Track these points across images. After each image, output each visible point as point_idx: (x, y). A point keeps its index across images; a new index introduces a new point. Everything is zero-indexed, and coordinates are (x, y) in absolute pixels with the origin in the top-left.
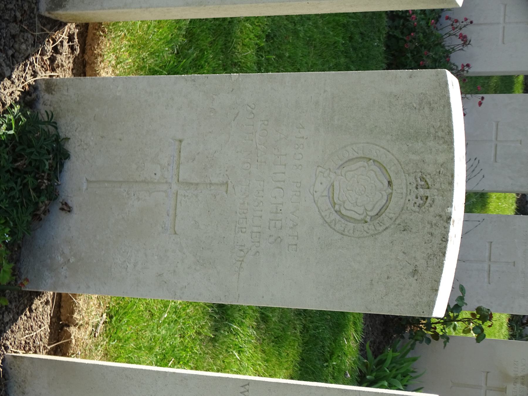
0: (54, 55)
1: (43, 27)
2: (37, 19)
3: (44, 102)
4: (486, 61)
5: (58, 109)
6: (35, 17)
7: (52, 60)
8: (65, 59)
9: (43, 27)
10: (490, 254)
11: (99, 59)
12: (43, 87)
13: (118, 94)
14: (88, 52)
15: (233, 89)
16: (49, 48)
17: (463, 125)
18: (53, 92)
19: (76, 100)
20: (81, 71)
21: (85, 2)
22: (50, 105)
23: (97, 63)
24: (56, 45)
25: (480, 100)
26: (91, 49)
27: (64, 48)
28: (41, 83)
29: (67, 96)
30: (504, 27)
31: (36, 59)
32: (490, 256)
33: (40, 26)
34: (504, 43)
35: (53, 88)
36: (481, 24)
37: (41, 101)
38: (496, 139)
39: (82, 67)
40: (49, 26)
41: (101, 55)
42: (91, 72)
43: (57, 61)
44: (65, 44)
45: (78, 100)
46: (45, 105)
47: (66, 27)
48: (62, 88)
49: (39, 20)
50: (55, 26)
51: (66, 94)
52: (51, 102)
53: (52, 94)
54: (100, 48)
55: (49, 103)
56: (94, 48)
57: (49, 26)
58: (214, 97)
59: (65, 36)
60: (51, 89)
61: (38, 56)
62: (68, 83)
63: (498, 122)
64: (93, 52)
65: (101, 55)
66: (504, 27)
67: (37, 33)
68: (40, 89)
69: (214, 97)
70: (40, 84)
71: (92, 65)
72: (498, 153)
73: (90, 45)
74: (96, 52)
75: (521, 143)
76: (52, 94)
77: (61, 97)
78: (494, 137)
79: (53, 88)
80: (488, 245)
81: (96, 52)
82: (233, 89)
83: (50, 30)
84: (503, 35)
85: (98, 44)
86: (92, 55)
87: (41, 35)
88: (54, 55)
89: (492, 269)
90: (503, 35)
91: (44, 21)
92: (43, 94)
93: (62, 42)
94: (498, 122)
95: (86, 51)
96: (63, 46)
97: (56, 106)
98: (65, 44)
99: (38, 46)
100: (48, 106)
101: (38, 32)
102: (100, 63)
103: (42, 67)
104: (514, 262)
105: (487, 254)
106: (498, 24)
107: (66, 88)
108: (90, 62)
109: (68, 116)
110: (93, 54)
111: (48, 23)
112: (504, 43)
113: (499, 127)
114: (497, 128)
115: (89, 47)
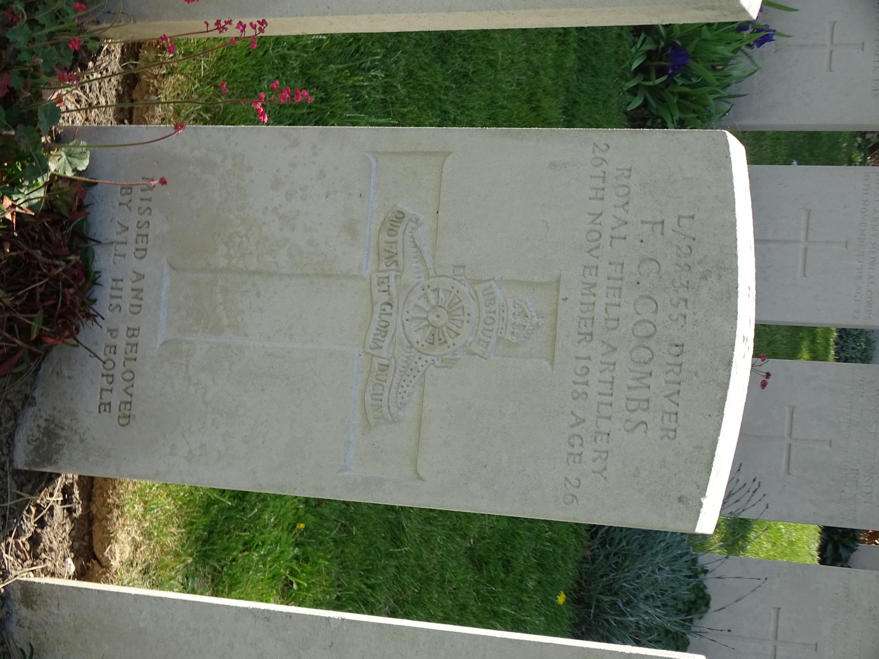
0: (39, 531)
1: (19, 492)
2: (9, 479)
3: (19, 620)
4: (808, 90)
5: (42, 636)
6: (6, 476)
7: (35, 540)
8: (58, 534)
9: (19, 492)
10: (777, 627)
11: (116, 512)
12: (19, 594)
13: (142, 625)
14: (98, 500)
15: (332, 644)
16: (29, 525)
17: (754, 271)
18: (35, 607)
19: (72, 624)
20: (85, 532)
21: (90, 460)
22: (29, 628)
23: (111, 520)
24: (42, 517)
25: (764, 379)
26: (101, 495)
27: (54, 518)
28: (15, 588)
29: (58, 615)
30: (790, 446)
31: (7, 545)
32: (777, 632)
33: (15, 491)
34: (805, 276)
35: (34, 598)
36: (768, 241)
37: (14, 618)
38: (790, 435)
39: (86, 524)
40: (30, 486)
41: (118, 507)
42: (101, 533)
43: (42, 545)
44: (58, 509)
45: (75, 626)
46: (21, 626)
47: (60, 480)
48: (49, 601)
49: (13, 478)
50: (40, 482)
51: (56, 612)
52: (31, 621)
53: (32, 609)
54: (117, 494)
55: (27, 624)
56: (107, 494)
57: (30, 486)
58: (301, 652)
59: (58, 497)
60: (32, 601)
61: (11, 540)
62: (60, 594)
63: (794, 407)
64: (105, 501)
65: (118, 507)
66: (806, 249)
67: (8, 504)
68: (12, 597)
69: (301, 652)
70: (13, 589)
71: (104, 522)
72: (792, 458)
73: (101, 488)
74: (110, 501)
75: (830, 446)
76: (32, 609)
77: (47, 617)
78: (786, 433)
79: (34, 598)
80: (773, 613)
81: (110, 501)
82: (332, 644)
83: (32, 494)
84: (805, 261)
85: (115, 488)
86: (103, 506)
87: (16, 504)
88: (39, 531)
89: (779, 653)
90: (805, 261)
91: (22, 478)
92: (17, 607)
93: (51, 509)
94: (794, 407)
95: (94, 499)
96: (52, 516)
97: (38, 630)
98: (58, 509)
99: (10, 525)
100: (26, 629)
101: (12, 500)
102: (117, 519)
103: (18, 557)
104: (816, 645)
105: (772, 628)
106: (798, 242)
107: (56, 602)
108: (100, 517)
109: (59, 650)
110: (104, 504)
111: (29, 481)
112: (805, 276)
113: (795, 415)
114: (792, 417)
115: (99, 491)
